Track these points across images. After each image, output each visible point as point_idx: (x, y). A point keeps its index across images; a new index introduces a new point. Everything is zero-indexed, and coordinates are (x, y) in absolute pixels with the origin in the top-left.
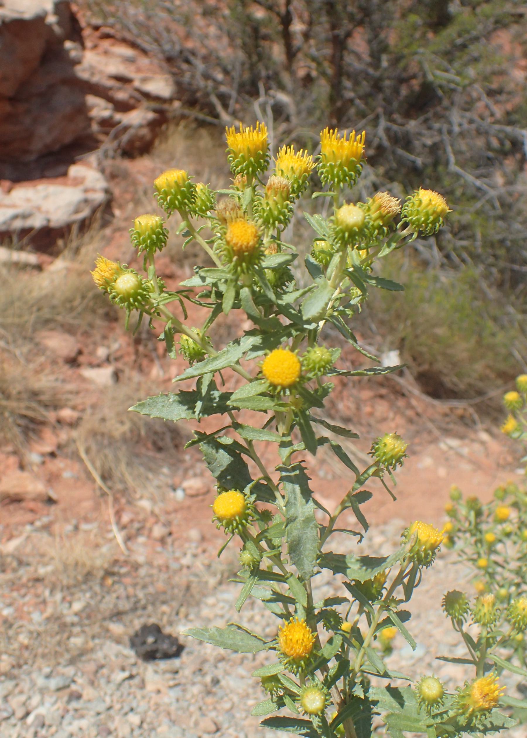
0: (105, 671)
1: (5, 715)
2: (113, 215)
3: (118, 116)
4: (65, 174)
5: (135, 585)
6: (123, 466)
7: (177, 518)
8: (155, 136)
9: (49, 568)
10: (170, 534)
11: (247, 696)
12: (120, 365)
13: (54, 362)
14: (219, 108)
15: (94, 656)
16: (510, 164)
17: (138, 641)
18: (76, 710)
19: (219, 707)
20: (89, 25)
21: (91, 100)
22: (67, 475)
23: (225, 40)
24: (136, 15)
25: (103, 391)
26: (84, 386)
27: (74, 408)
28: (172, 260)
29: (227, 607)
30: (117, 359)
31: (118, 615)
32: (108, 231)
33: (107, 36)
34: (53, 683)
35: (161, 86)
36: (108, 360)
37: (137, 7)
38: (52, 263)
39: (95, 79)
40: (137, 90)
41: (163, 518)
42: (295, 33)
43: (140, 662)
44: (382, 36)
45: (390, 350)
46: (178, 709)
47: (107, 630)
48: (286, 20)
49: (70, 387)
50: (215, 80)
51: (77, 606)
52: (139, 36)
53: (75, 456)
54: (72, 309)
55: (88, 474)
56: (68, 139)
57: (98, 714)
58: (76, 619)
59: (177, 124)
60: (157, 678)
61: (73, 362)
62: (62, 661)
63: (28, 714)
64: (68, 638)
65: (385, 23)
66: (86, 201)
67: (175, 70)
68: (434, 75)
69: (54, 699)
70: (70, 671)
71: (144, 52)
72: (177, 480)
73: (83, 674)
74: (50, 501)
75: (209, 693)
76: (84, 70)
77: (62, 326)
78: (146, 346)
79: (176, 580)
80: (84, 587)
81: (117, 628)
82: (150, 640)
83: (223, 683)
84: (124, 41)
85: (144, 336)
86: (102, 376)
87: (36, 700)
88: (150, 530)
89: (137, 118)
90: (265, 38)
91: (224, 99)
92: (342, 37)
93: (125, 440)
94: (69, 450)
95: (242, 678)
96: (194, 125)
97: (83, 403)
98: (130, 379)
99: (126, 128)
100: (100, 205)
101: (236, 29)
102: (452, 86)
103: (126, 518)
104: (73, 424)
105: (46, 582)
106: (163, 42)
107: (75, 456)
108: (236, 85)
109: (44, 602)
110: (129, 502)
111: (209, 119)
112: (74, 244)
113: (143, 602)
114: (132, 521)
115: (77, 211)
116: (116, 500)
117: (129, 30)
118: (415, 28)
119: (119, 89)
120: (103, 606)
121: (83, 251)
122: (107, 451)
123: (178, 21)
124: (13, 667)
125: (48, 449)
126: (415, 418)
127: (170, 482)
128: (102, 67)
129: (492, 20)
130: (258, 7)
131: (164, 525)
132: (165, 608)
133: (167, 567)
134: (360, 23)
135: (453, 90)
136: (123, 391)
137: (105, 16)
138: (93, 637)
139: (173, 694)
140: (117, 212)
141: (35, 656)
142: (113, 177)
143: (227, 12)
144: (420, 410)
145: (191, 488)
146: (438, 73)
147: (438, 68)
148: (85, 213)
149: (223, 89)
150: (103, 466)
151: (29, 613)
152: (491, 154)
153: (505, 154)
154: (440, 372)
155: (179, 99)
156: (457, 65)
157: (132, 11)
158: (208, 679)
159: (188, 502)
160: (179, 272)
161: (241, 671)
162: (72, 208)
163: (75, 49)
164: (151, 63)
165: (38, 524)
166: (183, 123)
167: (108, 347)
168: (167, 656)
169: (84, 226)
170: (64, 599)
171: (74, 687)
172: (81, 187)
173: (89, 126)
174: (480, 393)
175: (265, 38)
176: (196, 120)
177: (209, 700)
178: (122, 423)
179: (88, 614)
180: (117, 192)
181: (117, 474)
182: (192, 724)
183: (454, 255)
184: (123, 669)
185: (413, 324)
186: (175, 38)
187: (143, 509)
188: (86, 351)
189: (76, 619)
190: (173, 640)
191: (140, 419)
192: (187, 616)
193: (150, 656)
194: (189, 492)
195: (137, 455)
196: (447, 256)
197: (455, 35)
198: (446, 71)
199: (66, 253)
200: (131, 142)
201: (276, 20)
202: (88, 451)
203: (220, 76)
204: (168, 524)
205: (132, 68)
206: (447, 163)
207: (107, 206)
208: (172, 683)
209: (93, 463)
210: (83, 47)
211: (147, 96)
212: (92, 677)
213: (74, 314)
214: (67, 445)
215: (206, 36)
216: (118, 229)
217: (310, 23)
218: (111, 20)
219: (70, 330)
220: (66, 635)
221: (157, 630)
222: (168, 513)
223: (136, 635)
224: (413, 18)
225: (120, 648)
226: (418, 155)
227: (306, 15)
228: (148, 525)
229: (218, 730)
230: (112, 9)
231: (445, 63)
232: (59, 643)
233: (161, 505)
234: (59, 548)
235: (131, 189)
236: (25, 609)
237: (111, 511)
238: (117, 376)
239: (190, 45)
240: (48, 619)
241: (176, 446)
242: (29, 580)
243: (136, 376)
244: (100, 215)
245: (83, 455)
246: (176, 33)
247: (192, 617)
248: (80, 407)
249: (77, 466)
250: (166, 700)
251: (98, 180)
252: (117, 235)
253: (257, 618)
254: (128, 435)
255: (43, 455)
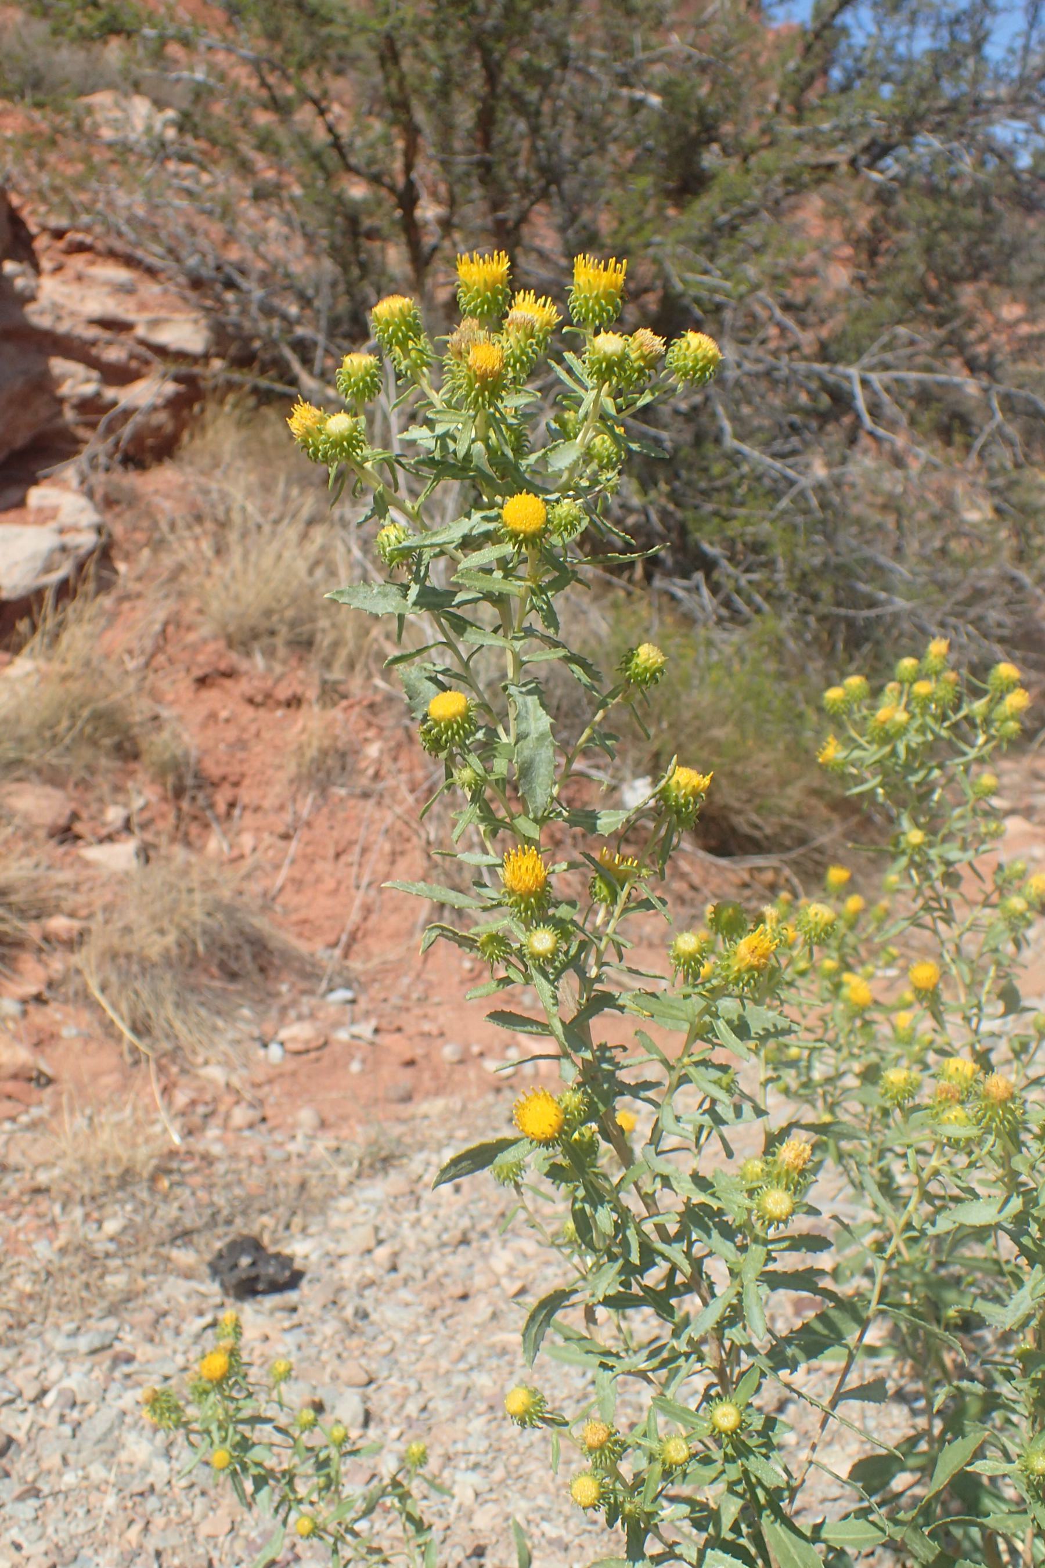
0: (170, 1319)
1: (6, 1396)
2: (115, 572)
3: (110, 393)
4: (21, 504)
5: (210, 1187)
6: (169, 1010)
7: (274, 1093)
8: (181, 425)
9: (56, 1172)
10: (264, 1120)
11: (418, 1330)
12: (149, 837)
13: (27, 836)
14: (297, 367)
15: (149, 1301)
16: (835, 433)
17: (224, 1264)
18: (128, 1376)
19: (370, 1351)
20: (44, 229)
21: (59, 365)
22: (68, 1032)
23: (299, 243)
24: (129, 207)
25: (123, 880)
26: (91, 872)
27: (72, 915)
28: (230, 644)
29: (373, 1211)
30: (144, 826)
31: (184, 1236)
32: (107, 602)
33: (80, 248)
34: (83, 1343)
35: (185, 333)
36: (127, 826)
37: (131, 192)
38: (10, 663)
39: (63, 328)
40: (142, 342)
41: (248, 1095)
42: (426, 223)
43: (230, 1301)
44: (586, 216)
45: (636, 776)
46: (301, 1360)
47: (168, 1259)
48: (408, 199)
49: (65, 876)
50: (284, 317)
51: (112, 1226)
52: (138, 244)
53: (84, 998)
54: (55, 740)
55: (108, 1027)
56: (21, 440)
57: (166, 1378)
58: (112, 1247)
59: (221, 402)
60: (261, 1320)
61: (66, 834)
62: (95, 1311)
63: (44, 1392)
64: (102, 1277)
65: (587, 195)
66: (63, 549)
67: (209, 303)
68: (684, 281)
69: (88, 1365)
70: (112, 1323)
71: (151, 272)
72: (268, 1027)
73: (132, 1328)
74: (42, 1080)
75: (352, 1331)
76: (42, 313)
77: (39, 771)
78: (194, 799)
79: (280, 1176)
80: (120, 1195)
81: (184, 1256)
82: (245, 1261)
83: (374, 1316)
84: (112, 254)
85: (189, 781)
86: (120, 856)
87: (56, 1370)
88: (228, 1116)
89: (146, 393)
90: (372, 234)
91: (303, 349)
92: (510, 224)
93: (168, 961)
94: (70, 989)
95: (407, 1305)
96: (251, 401)
97: (89, 905)
98: (168, 859)
99: (127, 413)
100: (91, 553)
101: (315, 219)
102: (719, 298)
103: (181, 1098)
104: (74, 943)
105: (54, 1193)
106: (183, 253)
107: (84, 998)
108: (323, 323)
109: (54, 1224)
110: (183, 1071)
111: (279, 387)
112: (50, 624)
113: (225, 1212)
114: (193, 1103)
115: (48, 569)
116: (161, 1069)
117: (120, 234)
118: (645, 198)
119: (109, 343)
120: (157, 1225)
121: (65, 639)
122: (138, 985)
123: (210, 213)
124: (10, 1327)
125: (32, 989)
126: (689, 894)
127: (256, 1033)
128: (72, 305)
129: (778, 178)
130: (355, 179)
131: (252, 1106)
132: (265, 1219)
133: (264, 1158)
134: (544, 195)
135: (719, 308)
136: (159, 874)
137: (74, 213)
138: (145, 1273)
139: (291, 1340)
140: (122, 567)
141: (47, 1308)
142: (109, 503)
143: (297, 191)
144: (696, 880)
145: (294, 1039)
146: (689, 276)
147: (692, 270)
148: (65, 569)
149: (300, 331)
150: (133, 1009)
151: (29, 1243)
152: (796, 418)
153: (824, 417)
154: (726, 807)
155: (220, 355)
156: (722, 261)
157: (122, 198)
158: (349, 1312)
159: (292, 1065)
160: (244, 665)
161: (404, 1294)
162: (39, 564)
163: (23, 274)
164: (165, 292)
165: (24, 1119)
166: (231, 398)
167: (126, 805)
168: (276, 1287)
169: (65, 591)
170: (87, 1216)
171: (118, 1346)
172: (53, 525)
173: (60, 413)
174: (802, 840)
175: (372, 234)
176: (255, 390)
177: (354, 1342)
178: (162, 932)
179: (129, 1242)
180: (118, 530)
181: (158, 1026)
182: (327, 1379)
183: (739, 602)
184: (201, 1314)
185: (671, 726)
186: (203, 243)
187: (212, 1081)
188: (85, 814)
189: (112, 1247)
190: (286, 1261)
191: (194, 923)
192: (304, 1230)
193: (247, 1289)
194: (292, 1046)
195: (194, 989)
196: (727, 603)
197: (716, 208)
198: (706, 272)
199: (37, 641)
200: (137, 438)
201: (391, 200)
202: (103, 989)
203: (293, 310)
204: (258, 1103)
205: (131, 303)
206: (718, 440)
207: (105, 553)
208: (287, 1324)
209: (115, 1007)
210: (38, 270)
211: (161, 351)
212: (149, 1331)
213: (60, 748)
214: (64, 980)
215: (264, 237)
216: (126, 597)
217: (452, 202)
218: (85, 219)
219: (53, 778)
220: (96, 1273)
221: (255, 1245)
222: (257, 1086)
223: (220, 1256)
224: (644, 182)
225: (194, 1285)
226: (665, 427)
227: (442, 189)
228: (222, 1109)
229: (370, 1382)
230: (84, 197)
231: (703, 261)
232: (87, 1286)
233: (244, 1072)
234: (69, 1141)
235: (145, 523)
236: (22, 1237)
237: (156, 1088)
238: (145, 854)
239: (234, 254)
240: (63, 1251)
241: (262, 970)
242: (22, 1193)
243: (180, 853)
244: (92, 571)
245: (97, 994)
246: (207, 234)
247: (313, 1230)
248: (84, 912)
249: (87, 1016)
250: (281, 1349)
251: (82, 511)
252: (126, 606)
253: (427, 1220)
254: (175, 951)
255: (24, 1001)
